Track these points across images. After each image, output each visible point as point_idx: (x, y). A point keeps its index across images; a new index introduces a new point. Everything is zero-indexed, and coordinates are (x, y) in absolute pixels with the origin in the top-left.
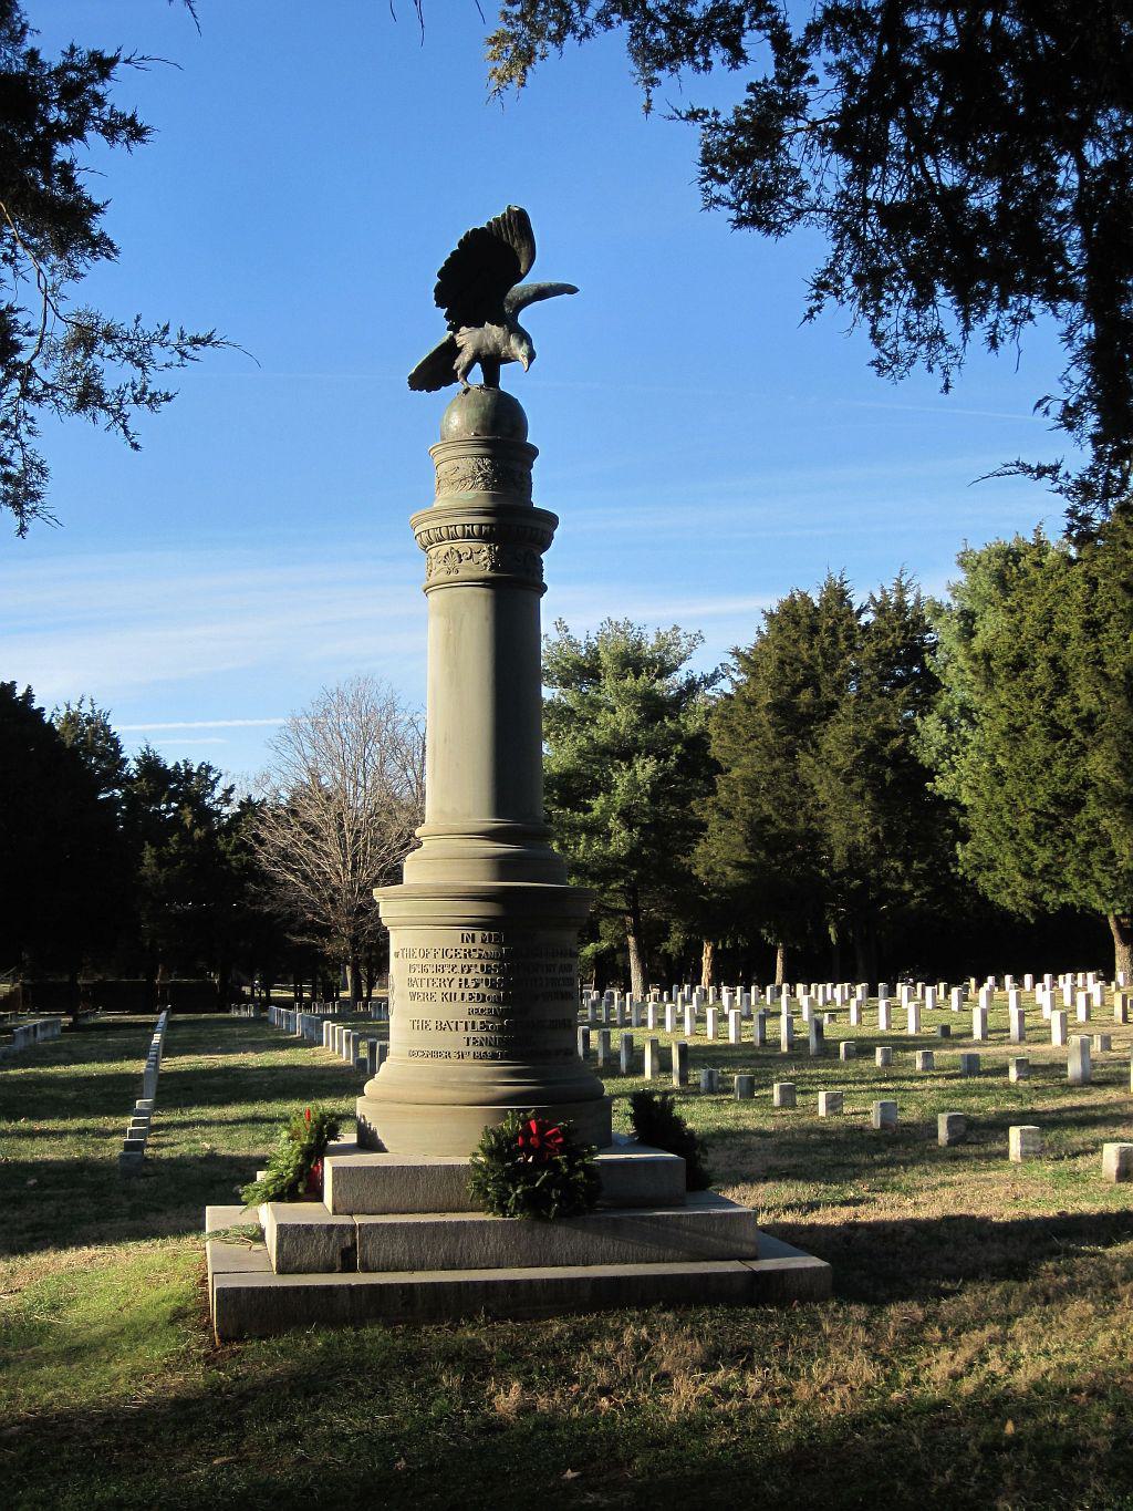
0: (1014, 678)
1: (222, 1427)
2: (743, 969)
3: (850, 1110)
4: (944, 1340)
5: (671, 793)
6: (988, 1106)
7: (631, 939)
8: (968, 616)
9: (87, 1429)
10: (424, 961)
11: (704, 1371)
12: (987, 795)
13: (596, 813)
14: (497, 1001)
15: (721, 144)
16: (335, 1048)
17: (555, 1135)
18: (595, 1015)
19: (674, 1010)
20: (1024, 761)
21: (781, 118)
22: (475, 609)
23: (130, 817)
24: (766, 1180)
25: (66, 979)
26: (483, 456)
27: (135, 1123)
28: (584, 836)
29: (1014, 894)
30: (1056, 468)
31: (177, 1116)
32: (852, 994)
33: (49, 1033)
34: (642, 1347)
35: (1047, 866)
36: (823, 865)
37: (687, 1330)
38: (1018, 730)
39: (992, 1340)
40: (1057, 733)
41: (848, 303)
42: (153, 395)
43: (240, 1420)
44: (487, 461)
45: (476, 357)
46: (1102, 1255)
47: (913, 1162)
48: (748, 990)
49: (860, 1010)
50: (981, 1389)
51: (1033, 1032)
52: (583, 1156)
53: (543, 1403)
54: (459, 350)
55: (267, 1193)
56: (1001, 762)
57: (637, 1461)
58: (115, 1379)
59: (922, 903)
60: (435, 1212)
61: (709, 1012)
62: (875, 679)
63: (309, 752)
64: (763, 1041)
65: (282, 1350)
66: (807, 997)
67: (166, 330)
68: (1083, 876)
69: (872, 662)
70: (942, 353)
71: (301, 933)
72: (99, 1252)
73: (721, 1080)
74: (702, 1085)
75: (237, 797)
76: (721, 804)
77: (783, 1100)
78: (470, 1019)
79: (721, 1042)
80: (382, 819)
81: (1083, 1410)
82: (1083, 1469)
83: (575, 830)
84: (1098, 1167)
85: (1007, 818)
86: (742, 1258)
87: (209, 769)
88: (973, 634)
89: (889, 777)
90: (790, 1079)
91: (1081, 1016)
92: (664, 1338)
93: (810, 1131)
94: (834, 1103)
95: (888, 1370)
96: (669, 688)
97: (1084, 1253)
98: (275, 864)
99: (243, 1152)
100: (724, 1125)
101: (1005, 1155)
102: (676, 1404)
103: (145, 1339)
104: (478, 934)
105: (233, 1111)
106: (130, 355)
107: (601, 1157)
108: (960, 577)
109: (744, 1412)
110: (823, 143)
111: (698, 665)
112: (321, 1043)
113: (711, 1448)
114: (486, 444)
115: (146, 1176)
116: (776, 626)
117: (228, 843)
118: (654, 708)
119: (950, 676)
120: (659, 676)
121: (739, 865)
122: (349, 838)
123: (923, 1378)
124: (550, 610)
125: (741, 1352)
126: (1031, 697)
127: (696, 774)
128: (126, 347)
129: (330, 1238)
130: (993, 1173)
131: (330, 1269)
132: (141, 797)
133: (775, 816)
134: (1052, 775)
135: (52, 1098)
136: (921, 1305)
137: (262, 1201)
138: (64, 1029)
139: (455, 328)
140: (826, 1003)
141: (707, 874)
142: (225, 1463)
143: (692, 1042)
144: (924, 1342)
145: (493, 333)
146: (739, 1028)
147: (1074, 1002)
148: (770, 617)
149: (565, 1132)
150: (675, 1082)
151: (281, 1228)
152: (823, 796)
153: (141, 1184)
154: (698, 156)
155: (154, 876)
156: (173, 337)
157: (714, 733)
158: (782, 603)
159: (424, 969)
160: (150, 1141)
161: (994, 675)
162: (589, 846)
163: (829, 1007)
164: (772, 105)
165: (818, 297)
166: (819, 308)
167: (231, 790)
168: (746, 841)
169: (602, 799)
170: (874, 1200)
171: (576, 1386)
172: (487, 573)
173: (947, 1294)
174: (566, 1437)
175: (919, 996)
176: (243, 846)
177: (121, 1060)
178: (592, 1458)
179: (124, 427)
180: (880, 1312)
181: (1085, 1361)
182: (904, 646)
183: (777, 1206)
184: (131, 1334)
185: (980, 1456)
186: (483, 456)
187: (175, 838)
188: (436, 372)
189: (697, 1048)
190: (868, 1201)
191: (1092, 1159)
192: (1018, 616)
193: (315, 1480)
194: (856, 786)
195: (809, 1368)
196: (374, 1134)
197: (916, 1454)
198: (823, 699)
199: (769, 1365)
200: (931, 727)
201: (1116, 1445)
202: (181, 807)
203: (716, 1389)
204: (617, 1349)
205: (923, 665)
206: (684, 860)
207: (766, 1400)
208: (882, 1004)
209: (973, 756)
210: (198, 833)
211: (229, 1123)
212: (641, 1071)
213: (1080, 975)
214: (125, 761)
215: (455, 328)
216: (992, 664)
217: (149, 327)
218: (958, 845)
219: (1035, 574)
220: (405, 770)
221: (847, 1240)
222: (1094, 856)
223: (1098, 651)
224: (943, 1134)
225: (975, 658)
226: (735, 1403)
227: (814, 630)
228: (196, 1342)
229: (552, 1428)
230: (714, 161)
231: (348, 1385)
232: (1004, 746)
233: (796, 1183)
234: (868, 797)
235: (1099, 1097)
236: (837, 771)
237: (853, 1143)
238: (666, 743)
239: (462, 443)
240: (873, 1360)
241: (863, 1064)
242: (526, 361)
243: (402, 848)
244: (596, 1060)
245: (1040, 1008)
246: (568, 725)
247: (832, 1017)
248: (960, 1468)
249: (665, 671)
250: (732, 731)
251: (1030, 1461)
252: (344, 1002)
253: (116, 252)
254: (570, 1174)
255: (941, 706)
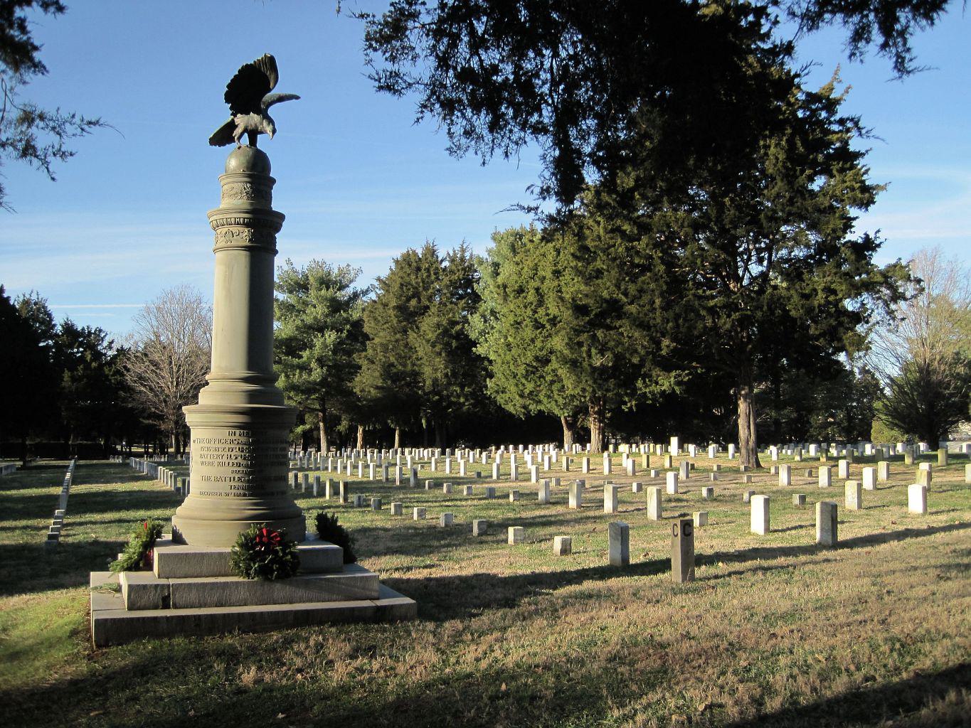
0: (518, 297)
1: (96, 695)
2: (379, 440)
3: (430, 517)
4: (473, 640)
5: (343, 350)
6: (497, 515)
7: (321, 424)
8: (496, 265)
9: (20, 699)
10: (209, 445)
11: (351, 659)
12: (503, 356)
13: (305, 359)
14: (247, 466)
15: (376, 32)
16: (164, 481)
17: (276, 536)
18: (302, 464)
19: (342, 462)
20: (521, 339)
21: (406, 21)
22: (243, 259)
23: (56, 356)
24: (385, 554)
25: (20, 441)
26: (247, 182)
27: (54, 523)
28: (298, 371)
29: (515, 405)
30: (537, 208)
31: (78, 519)
32: (433, 454)
33: (9, 471)
34: (320, 646)
35: (531, 393)
36: (420, 388)
37: (343, 637)
38: (519, 324)
39: (496, 640)
40: (538, 325)
41: (437, 116)
42: (64, 153)
43: (105, 691)
44: (249, 185)
45: (245, 130)
46: (552, 594)
47: (460, 545)
48: (380, 452)
49: (436, 463)
50: (490, 666)
51: (523, 476)
52: (290, 547)
53: (267, 678)
54: (237, 126)
55: (123, 567)
56: (510, 339)
57: (315, 708)
58: (37, 670)
59: (469, 408)
60: (212, 576)
61: (360, 463)
62: (448, 295)
63: (155, 323)
64: (387, 479)
65: (130, 651)
66: (411, 455)
67: (73, 116)
68: (549, 397)
69: (448, 287)
70: (482, 145)
71: (148, 418)
72: (32, 597)
73: (365, 500)
74: (355, 503)
75: (115, 346)
76: (369, 356)
77: (396, 511)
78: (232, 476)
79: (365, 479)
80: (193, 359)
81: (540, 676)
82: (539, 708)
83: (293, 367)
84: (552, 546)
85: (512, 367)
86: (372, 599)
87: (100, 331)
88: (498, 274)
89: (454, 344)
90: (401, 500)
91: (546, 467)
92: (330, 641)
93: (409, 528)
94: (422, 514)
95: (444, 657)
96: (343, 296)
97: (543, 593)
98: (135, 382)
99: (113, 539)
100: (366, 525)
101: (506, 541)
102: (336, 677)
103: (55, 646)
104: (238, 432)
105: (109, 516)
106: (53, 128)
107: (300, 547)
108: (492, 245)
109: (370, 681)
110: (427, 35)
111: (359, 285)
112: (157, 478)
113: (354, 700)
114: (249, 176)
115: (59, 553)
116: (399, 267)
117: (110, 370)
118: (336, 306)
119: (486, 295)
120: (339, 289)
121: (377, 388)
122: (175, 369)
123: (461, 661)
124: (279, 262)
125: (370, 649)
126: (525, 307)
127: (356, 340)
128: (51, 124)
129: (156, 591)
130: (499, 551)
131: (156, 607)
132: (63, 345)
133: (396, 363)
134: (535, 347)
135: (9, 508)
136: (462, 622)
137: (120, 571)
138: (18, 469)
139: (234, 115)
140: (420, 459)
141: (361, 391)
142: (97, 715)
143: (350, 479)
144: (462, 641)
145: (254, 118)
146: (375, 472)
147: (543, 460)
148: (397, 262)
149: (282, 535)
150: (341, 501)
151: (130, 586)
152: (420, 354)
153: (57, 557)
154: (363, 36)
155: (70, 387)
156: (77, 120)
157: (366, 320)
158: (403, 256)
159: (209, 449)
160: (63, 533)
161: (508, 295)
162: (301, 376)
163: (421, 461)
164: (402, 14)
165: (422, 112)
166: (422, 118)
167: (112, 342)
168: (381, 375)
169: (308, 352)
170: (440, 565)
171: (285, 668)
172: (247, 243)
173: (474, 616)
174: (279, 696)
175: (466, 456)
176: (118, 372)
177: (49, 487)
178: (292, 706)
179: (47, 168)
180: (441, 626)
181: (541, 651)
182: (464, 279)
183: (391, 569)
184: (47, 644)
185: (489, 702)
186: (247, 182)
187: (82, 366)
188: (224, 136)
189: (353, 483)
190: (437, 566)
191: (549, 544)
192: (521, 266)
193: (145, 723)
194: (437, 349)
195: (404, 657)
196: (181, 535)
197: (457, 701)
198: (422, 304)
199: (384, 655)
200: (476, 320)
201: (555, 694)
202: (85, 350)
203: (357, 669)
204: (306, 649)
205: (473, 289)
206: (349, 384)
207: (382, 673)
208: (448, 460)
209: (497, 335)
210: (94, 364)
211: (106, 523)
212: (324, 495)
213: (547, 445)
214: (55, 325)
215: (234, 115)
216: (507, 290)
217: (64, 114)
218: (488, 380)
219: (529, 246)
220: (205, 334)
221: (426, 587)
222: (555, 387)
223: (559, 286)
224: (476, 530)
225: (499, 287)
226: (366, 676)
227: (419, 269)
228: (82, 648)
229: (271, 691)
230: (371, 39)
231: (165, 670)
232: (512, 331)
233: (400, 556)
234: (443, 355)
235: (553, 511)
236: (428, 341)
237: (430, 535)
238: (341, 324)
239: (235, 174)
240: (437, 652)
241: (437, 492)
242: (271, 134)
243: (203, 374)
244: (301, 488)
245: (526, 463)
246: (291, 313)
247: (422, 467)
248: (479, 708)
249: (342, 288)
250: (375, 319)
251: (513, 703)
252: (170, 455)
253: (47, 72)
254: (283, 556)
255: (481, 310)
